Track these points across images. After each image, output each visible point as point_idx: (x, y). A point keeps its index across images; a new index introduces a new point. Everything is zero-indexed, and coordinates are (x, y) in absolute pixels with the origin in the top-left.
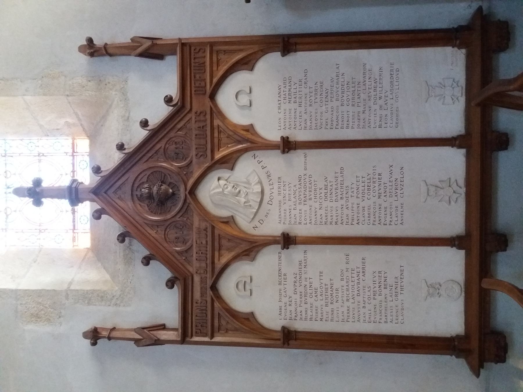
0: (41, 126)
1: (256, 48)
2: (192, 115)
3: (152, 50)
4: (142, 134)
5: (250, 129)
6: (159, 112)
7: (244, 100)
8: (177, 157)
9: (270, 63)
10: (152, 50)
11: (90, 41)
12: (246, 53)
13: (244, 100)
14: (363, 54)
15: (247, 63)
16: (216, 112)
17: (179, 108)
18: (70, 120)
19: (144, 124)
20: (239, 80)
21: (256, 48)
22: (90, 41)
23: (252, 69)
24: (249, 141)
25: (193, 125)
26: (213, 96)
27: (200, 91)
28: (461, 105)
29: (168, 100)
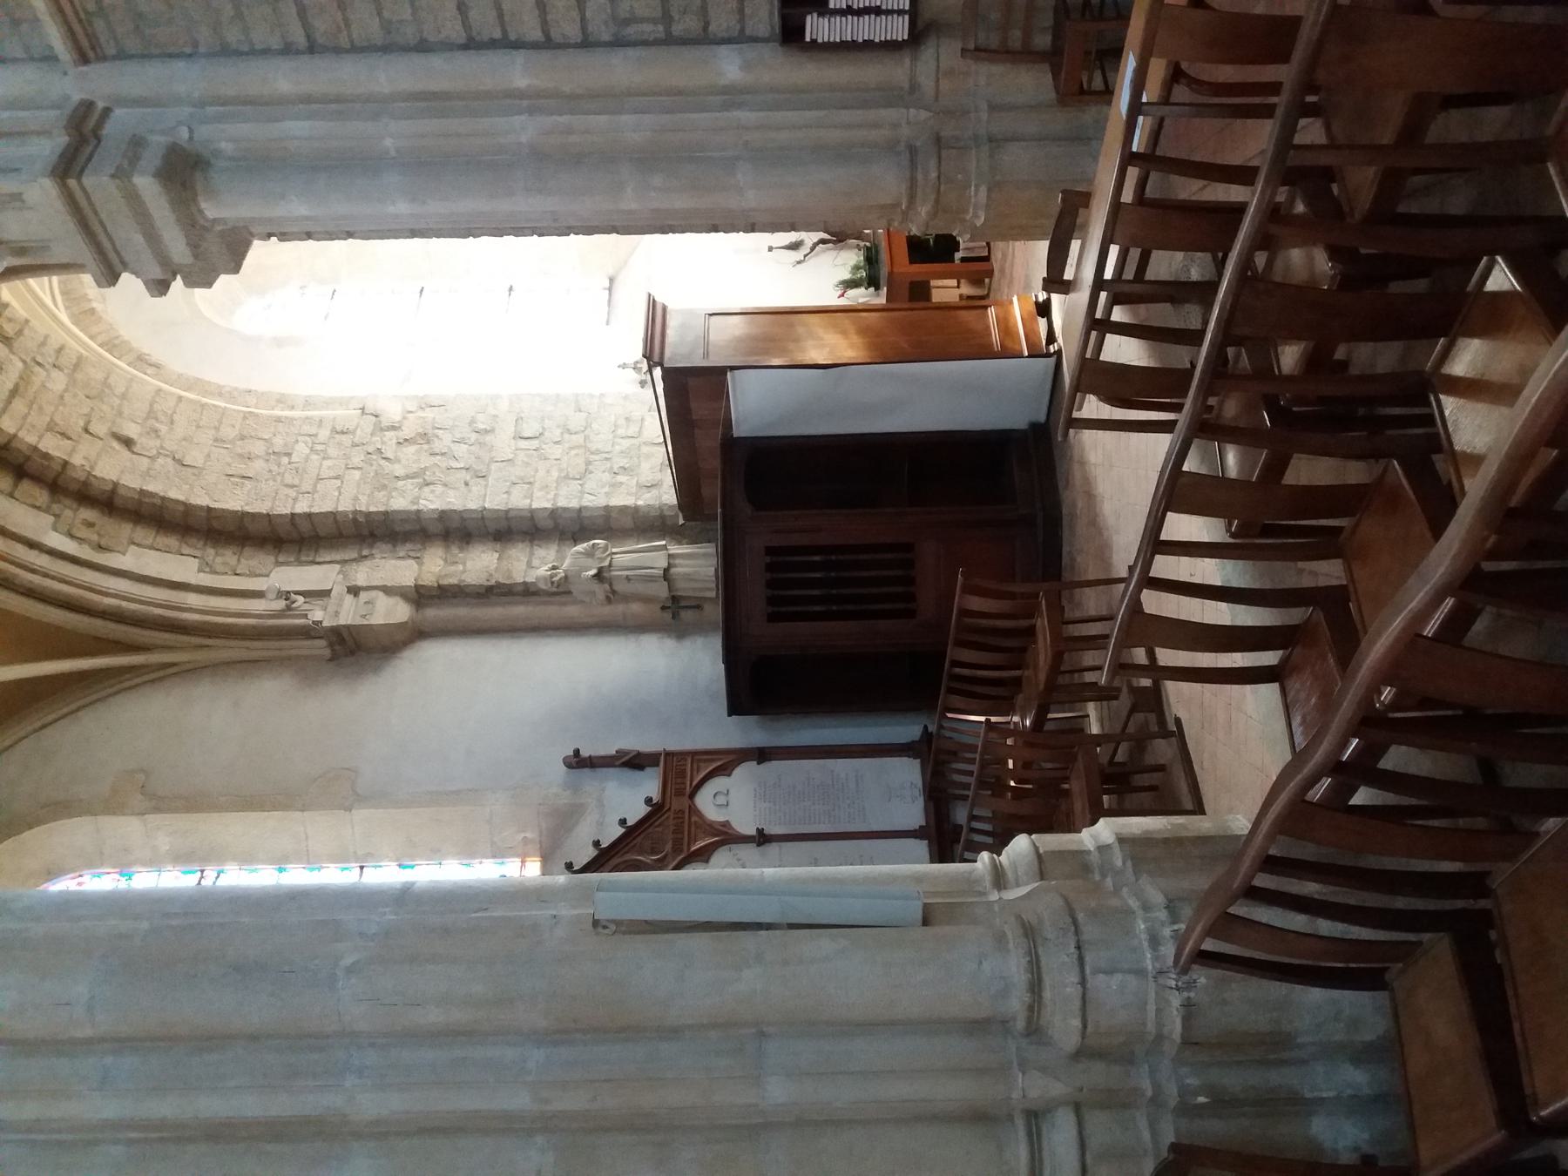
0: (493, 843)
1: (731, 757)
2: (671, 814)
3: (635, 762)
4: (619, 831)
5: (726, 824)
6: (636, 811)
7: (721, 800)
8: (653, 852)
9: (745, 772)
10: (635, 762)
11: (577, 752)
12: (725, 762)
13: (721, 800)
14: (830, 763)
15: (724, 770)
16: (694, 810)
17: (656, 810)
18: (529, 835)
19: (623, 822)
20: (718, 783)
21: (731, 757)
22: (577, 752)
23: (707, 861)
24: (726, 837)
25: (671, 822)
26: (692, 796)
27: (680, 793)
28: (920, 803)
29: (648, 801)
